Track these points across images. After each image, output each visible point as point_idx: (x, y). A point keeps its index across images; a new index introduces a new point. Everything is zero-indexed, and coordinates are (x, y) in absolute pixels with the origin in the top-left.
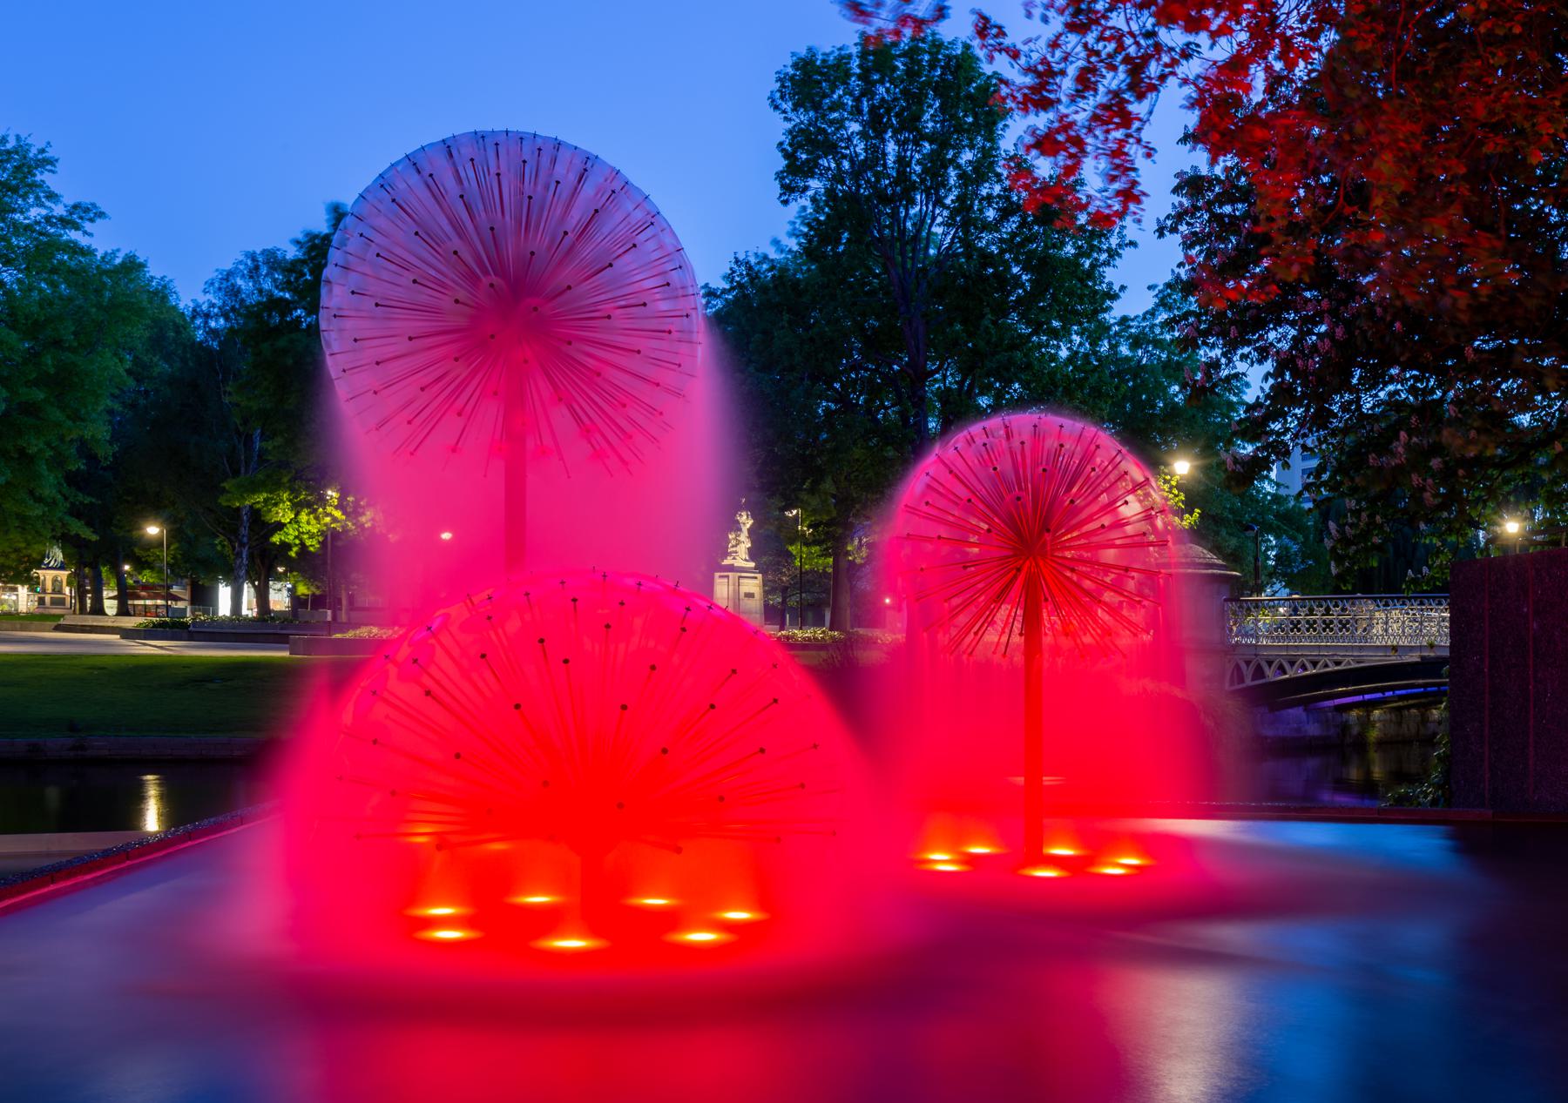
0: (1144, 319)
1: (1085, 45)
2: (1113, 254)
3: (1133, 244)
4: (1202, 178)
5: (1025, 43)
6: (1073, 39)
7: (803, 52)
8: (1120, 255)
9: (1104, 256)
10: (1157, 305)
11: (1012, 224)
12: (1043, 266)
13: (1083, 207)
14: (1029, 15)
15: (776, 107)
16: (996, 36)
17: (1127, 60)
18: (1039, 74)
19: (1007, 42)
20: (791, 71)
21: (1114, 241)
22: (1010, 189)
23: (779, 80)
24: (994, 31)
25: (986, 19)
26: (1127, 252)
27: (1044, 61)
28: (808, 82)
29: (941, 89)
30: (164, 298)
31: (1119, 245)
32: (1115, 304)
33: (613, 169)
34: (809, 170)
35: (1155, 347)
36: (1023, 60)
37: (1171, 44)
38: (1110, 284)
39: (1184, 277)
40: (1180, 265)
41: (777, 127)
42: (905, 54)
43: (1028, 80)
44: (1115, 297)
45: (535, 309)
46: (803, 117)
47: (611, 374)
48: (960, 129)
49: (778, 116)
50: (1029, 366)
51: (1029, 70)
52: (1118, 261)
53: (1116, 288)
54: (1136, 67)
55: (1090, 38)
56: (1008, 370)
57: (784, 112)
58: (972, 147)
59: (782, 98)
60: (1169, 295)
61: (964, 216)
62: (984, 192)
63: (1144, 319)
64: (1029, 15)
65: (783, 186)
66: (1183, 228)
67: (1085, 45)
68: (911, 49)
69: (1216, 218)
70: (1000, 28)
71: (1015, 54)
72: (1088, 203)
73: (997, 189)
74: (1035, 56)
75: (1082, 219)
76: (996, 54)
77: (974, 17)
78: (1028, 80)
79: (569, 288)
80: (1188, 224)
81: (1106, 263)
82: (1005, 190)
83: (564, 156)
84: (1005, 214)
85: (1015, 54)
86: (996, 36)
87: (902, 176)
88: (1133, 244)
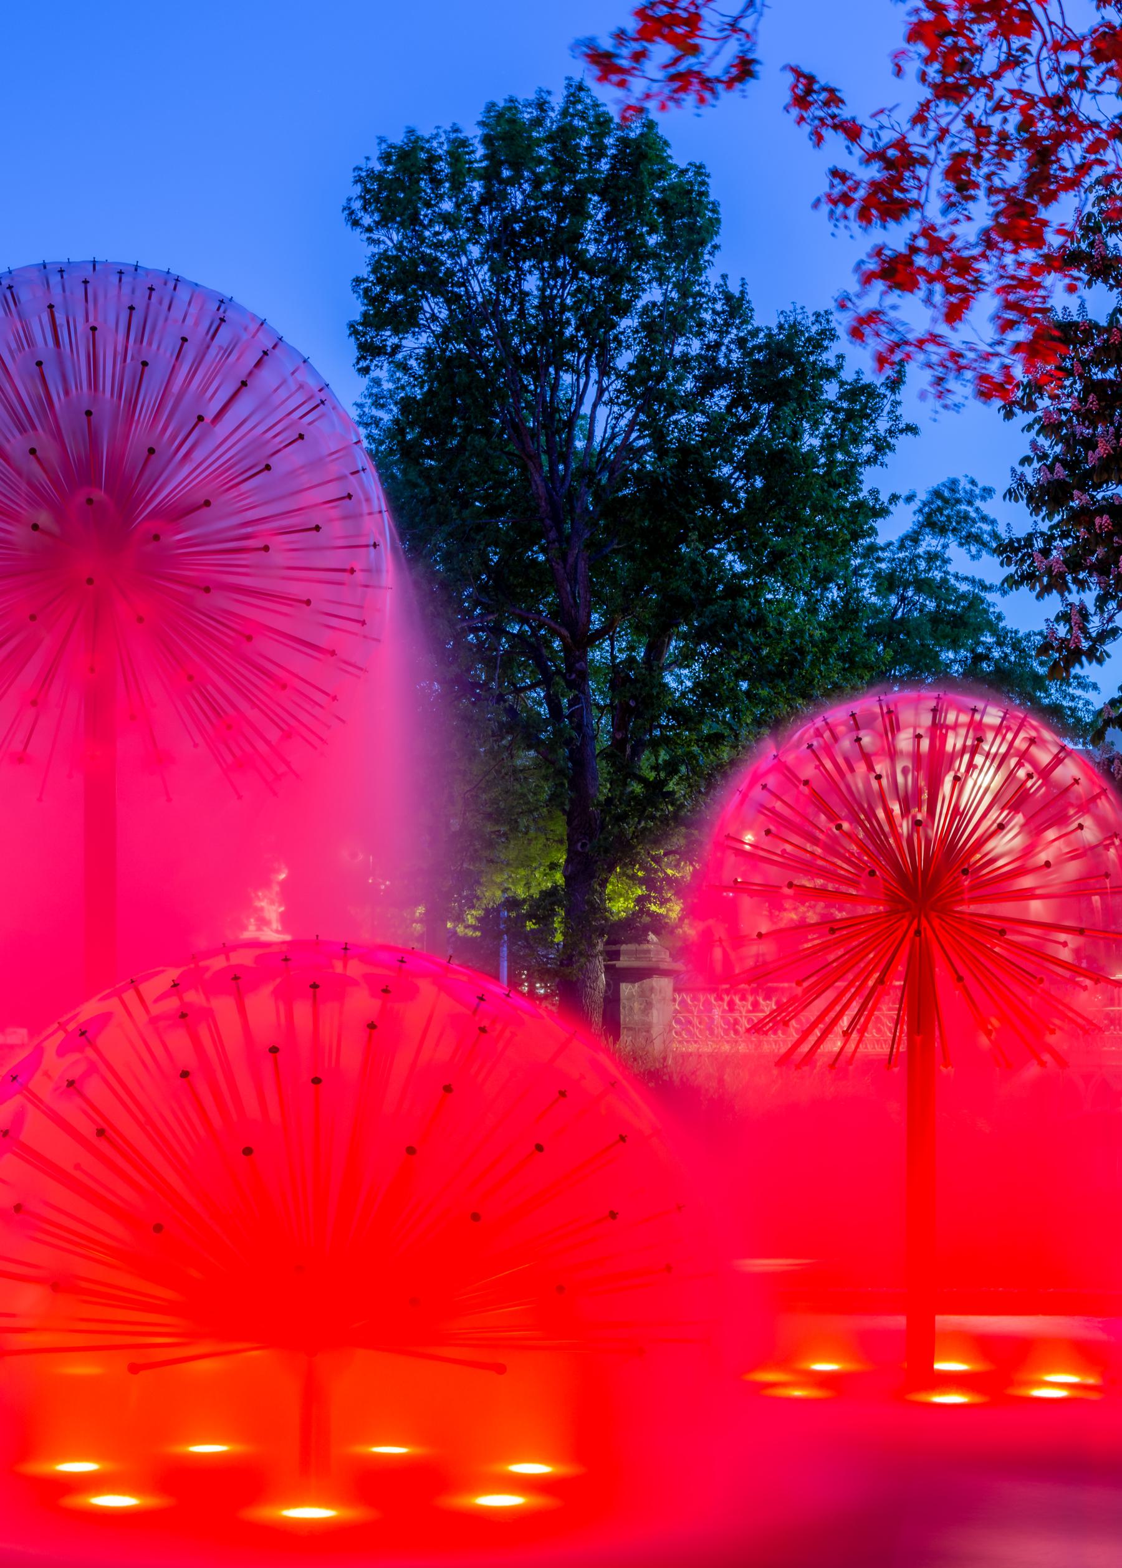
0: (902, 547)
1: (969, 118)
2: (882, 446)
3: (911, 429)
4: (1074, 324)
5: (874, 116)
6: (943, 108)
7: (398, 138)
8: (891, 448)
9: (867, 449)
10: (922, 526)
11: (720, 399)
12: (777, 464)
13: (830, 373)
14: (899, 71)
15: (356, 223)
16: (827, 104)
17: (1032, 142)
18: (889, 164)
19: (845, 113)
20: (378, 167)
21: (883, 425)
22: (717, 345)
23: (359, 180)
24: (824, 96)
25: (811, 79)
26: (902, 442)
27: (901, 144)
28: (398, 185)
29: (608, 189)
30: (412, 549)
31: (890, 432)
32: (879, 524)
33: (254, 317)
34: (405, 319)
35: (919, 590)
36: (867, 142)
37: (1095, 116)
38: (874, 492)
39: (1031, 481)
40: (1026, 460)
41: (357, 253)
42: (550, 138)
43: (874, 172)
44: (883, 512)
45: (156, 538)
46: (392, 238)
47: (265, 646)
48: (639, 253)
49: (358, 235)
50: (759, 622)
51: (876, 155)
52: (889, 458)
53: (884, 497)
54: (1042, 155)
55: (977, 105)
56: (728, 628)
57: (369, 230)
58: (661, 280)
59: (364, 209)
60: (940, 510)
61: (646, 389)
62: (678, 351)
63: (902, 547)
64: (899, 71)
65: (362, 347)
66: (1044, 403)
67: (969, 118)
68: (562, 129)
69: (1091, 386)
70: (832, 91)
71: (852, 131)
72: (840, 367)
73: (696, 347)
74: (887, 136)
75: (831, 391)
76: (828, 134)
77: (790, 78)
78: (874, 172)
79: (207, 503)
80: (1053, 397)
81: (871, 460)
82: (709, 347)
83: (183, 295)
84: (708, 384)
85: (852, 131)
86: (827, 104)
87: (547, 329)
88: (911, 429)
